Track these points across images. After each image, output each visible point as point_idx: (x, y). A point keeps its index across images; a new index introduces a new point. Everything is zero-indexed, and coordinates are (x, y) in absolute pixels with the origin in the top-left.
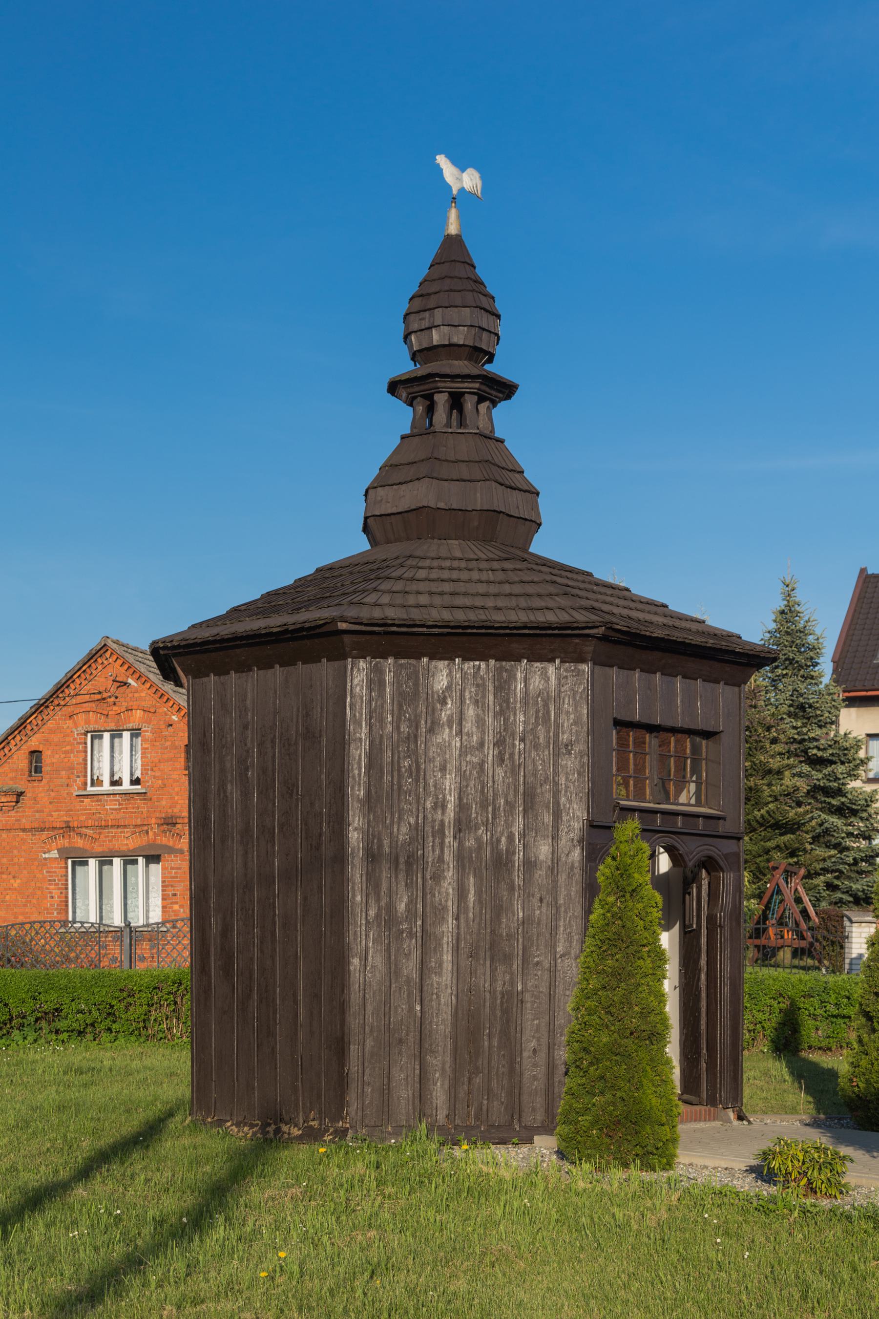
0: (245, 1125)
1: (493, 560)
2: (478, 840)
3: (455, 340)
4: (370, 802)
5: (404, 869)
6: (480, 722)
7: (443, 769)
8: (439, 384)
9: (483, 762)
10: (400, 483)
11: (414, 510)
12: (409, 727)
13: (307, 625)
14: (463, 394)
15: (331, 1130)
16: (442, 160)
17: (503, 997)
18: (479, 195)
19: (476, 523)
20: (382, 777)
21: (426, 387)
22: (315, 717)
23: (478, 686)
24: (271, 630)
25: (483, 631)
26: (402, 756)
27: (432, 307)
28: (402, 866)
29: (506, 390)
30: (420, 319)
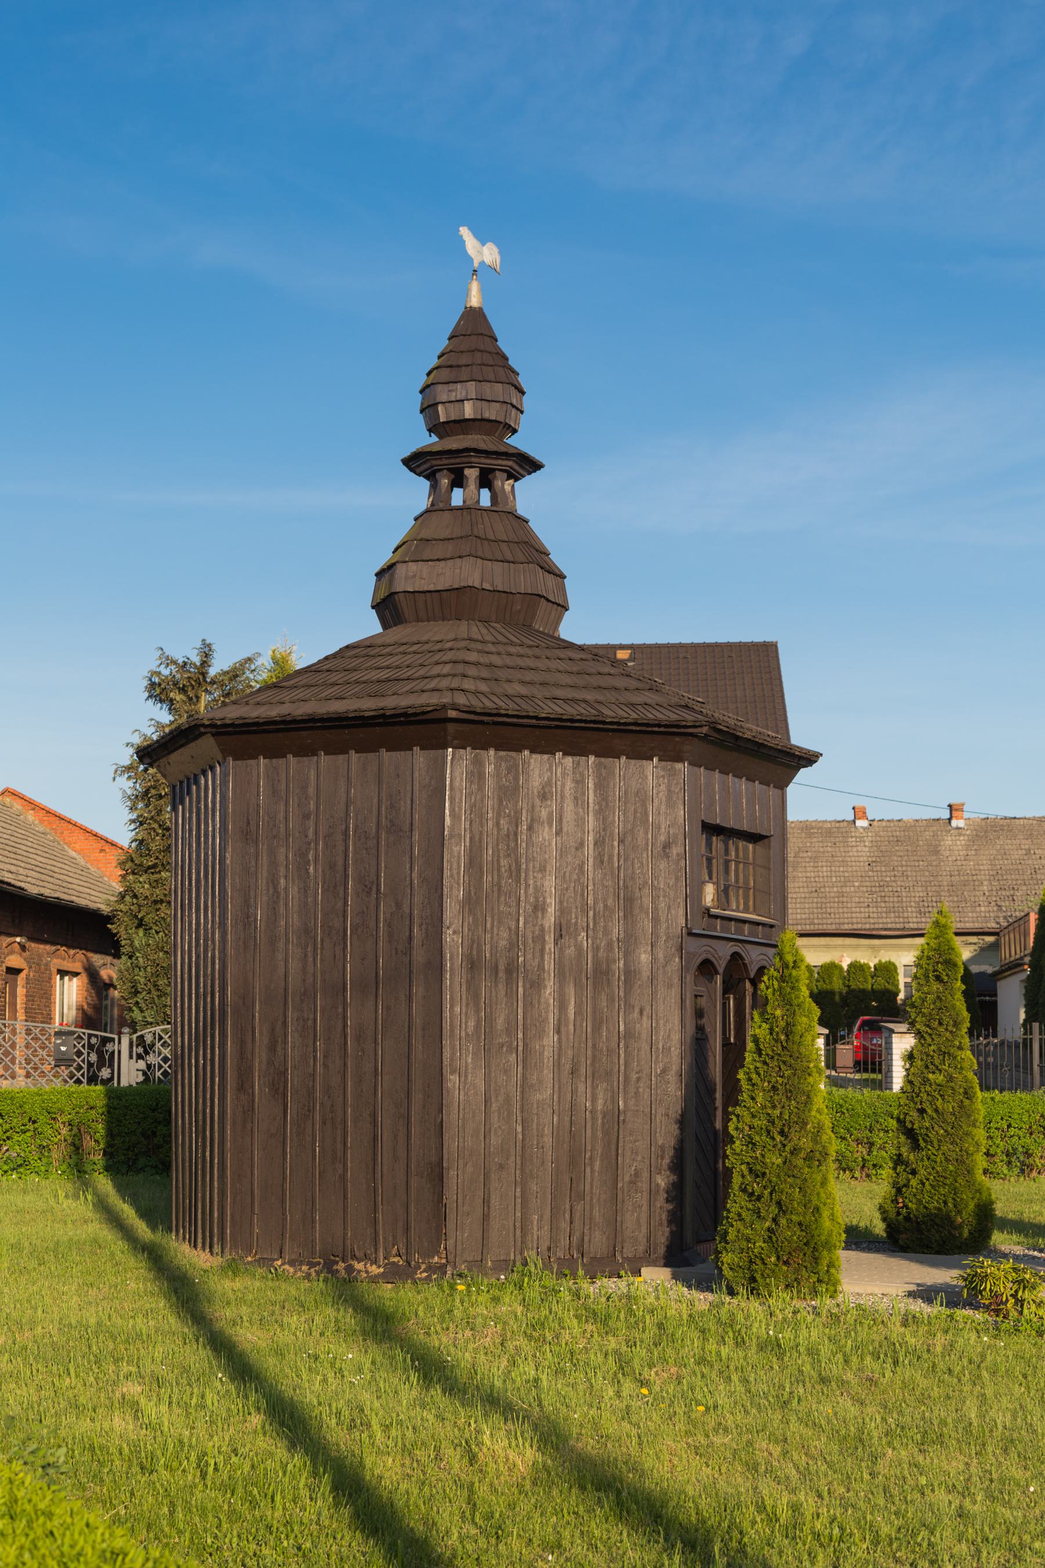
0: (301, 1263)
2: (579, 948)
3: (486, 415)
4: (470, 903)
5: (504, 977)
6: (580, 822)
7: (543, 869)
8: (473, 459)
9: (583, 863)
10: (438, 560)
11: (457, 589)
12: (510, 823)
13: (410, 711)
14: (495, 470)
15: (423, 1267)
16: (464, 232)
17: (604, 1117)
18: (498, 269)
19: (519, 607)
20: (481, 877)
21: (458, 460)
22: (403, 809)
23: (577, 782)
24: (362, 714)
25: (592, 725)
26: (501, 855)
27: (465, 379)
28: (502, 975)
29: (532, 465)
30: (450, 391)
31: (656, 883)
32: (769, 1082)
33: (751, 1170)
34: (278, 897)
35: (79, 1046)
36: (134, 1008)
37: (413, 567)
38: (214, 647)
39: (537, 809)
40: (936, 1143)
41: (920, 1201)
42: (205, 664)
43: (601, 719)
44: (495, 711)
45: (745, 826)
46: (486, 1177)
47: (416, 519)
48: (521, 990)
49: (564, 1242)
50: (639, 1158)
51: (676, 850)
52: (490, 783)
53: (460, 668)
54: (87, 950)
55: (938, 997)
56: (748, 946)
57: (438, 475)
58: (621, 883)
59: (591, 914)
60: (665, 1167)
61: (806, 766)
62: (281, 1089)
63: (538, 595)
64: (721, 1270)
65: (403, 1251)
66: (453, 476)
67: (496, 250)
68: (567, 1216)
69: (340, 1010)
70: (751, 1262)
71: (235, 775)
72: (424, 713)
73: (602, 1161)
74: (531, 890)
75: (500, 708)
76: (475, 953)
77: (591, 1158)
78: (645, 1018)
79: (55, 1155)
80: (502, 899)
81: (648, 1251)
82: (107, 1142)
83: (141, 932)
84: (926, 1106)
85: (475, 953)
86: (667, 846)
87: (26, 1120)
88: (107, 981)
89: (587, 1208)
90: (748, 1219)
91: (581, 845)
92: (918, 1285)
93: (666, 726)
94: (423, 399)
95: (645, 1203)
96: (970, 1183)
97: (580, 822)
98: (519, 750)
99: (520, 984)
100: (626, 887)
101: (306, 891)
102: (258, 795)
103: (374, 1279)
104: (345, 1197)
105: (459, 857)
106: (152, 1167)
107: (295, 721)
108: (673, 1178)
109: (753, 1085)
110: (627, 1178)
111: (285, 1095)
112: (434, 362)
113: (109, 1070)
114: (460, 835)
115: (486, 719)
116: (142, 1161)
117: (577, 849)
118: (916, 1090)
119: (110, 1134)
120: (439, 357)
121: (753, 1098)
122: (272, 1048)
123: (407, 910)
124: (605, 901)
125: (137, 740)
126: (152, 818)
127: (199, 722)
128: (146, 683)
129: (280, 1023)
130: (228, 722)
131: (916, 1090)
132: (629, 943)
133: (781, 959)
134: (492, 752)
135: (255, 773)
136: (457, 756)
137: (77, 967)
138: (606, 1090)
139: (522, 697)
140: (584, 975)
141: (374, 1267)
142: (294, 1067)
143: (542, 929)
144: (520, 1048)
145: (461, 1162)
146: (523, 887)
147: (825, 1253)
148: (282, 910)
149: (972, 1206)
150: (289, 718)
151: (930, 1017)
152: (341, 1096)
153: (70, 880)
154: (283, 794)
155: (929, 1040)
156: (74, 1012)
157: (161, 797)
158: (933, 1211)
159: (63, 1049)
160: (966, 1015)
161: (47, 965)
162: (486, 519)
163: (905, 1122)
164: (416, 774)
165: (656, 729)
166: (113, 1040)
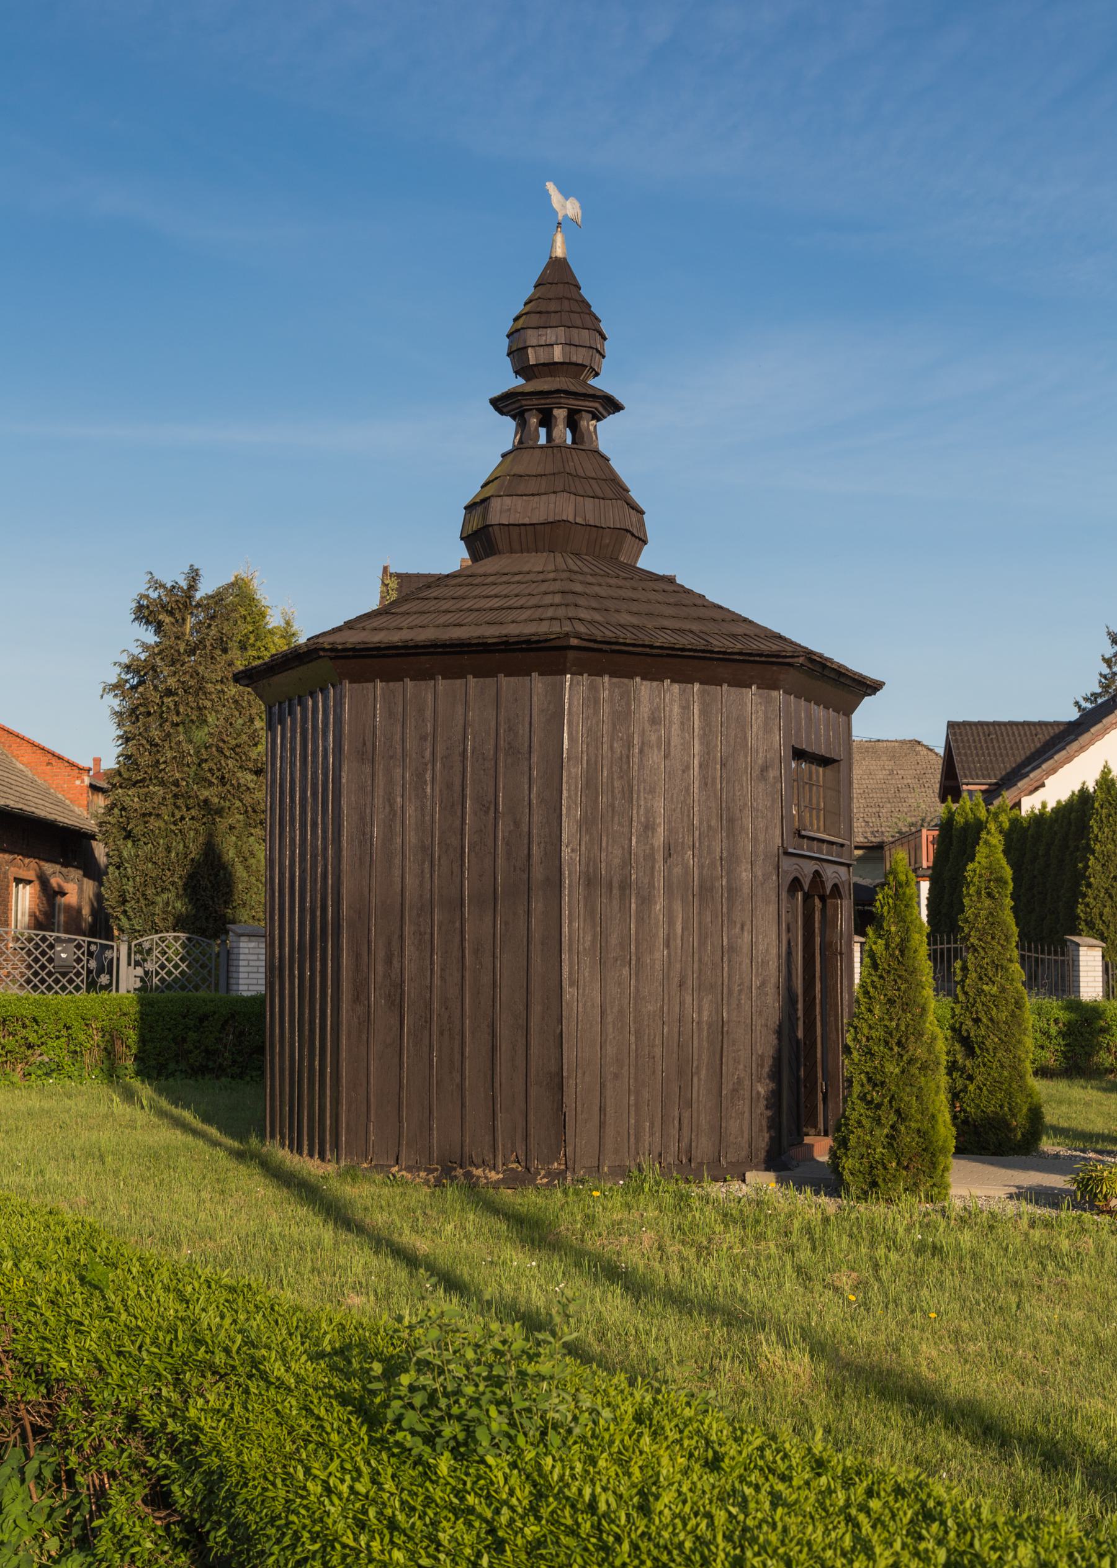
0: (419, 1169)
1: (575, 572)
2: (686, 867)
3: (574, 359)
4: (587, 823)
7: (652, 791)
9: (689, 785)
10: (533, 495)
13: (534, 638)
14: (581, 411)
15: (543, 1173)
16: (550, 187)
17: (709, 1028)
20: (597, 798)
21: (548, 401)
22: (521, 732)
28: (615, 891)
29: (612, 406)
31: (755, 805)
32: (885, 995)
33: (869, 1079)
34: (395, 815)
35: (79, 953)
36: (122, 917)
37: (508, 501)
38: (201, 572)
39: (647, 733)
40: (991, 1051)
41: (978, 1106)
42: (192, 587)
43: (709, 648)
44: (614, 640)
45: (823, 751)
46: (602, 1085)
47: (504, 456)
48: (633, 906)
49: (673, 1148)
50: (741, 1067)
51: (772, 774)
52: (605, 710)
53: (571, 598)
54: (40, 859)
55: (991, 913)
56: (825, 865)
57: (527, 415)
58: (724, 805)
59: (697, 833)
60: (765, 1075)
61: (870, 695)
62: (398, 1001)
63: (627, 531)
64: (840, 1175)
65: (522, 1158)
66: (541, 416)
67: (577, 205)
68: (676, 1123)
69: (458, 924)
70: (871, 1167)
71: (351, 698)
72: (546, 641)
73: (707, 1070)
74: (642, 811)
75: (618, 637)
76: (591, 870)
77: (697, 1067)
78: (746, 934)
79: (87, 1059)
80: (616, 818)
81: (750, 1156)
82: (139, 1048)
83: (130, 844)
84: (982, 1015)
85: (591, 870)
86: (764, 769)
87: (61, 1027)
88: (57, 889)
89: (695, 1115)
90: (868, 1126)
91: (687, 768)
92: (1018, 1187)
93: (767, 656)
94: (511, 342)
95: (747, 1109)
96: (1023, 1088)
97: (686, 746)
98: (631, 677)
99: (633, 901)
100: (728, 808)
101: (422, 810)
102: (375, 716)
103: (496, 1185)
104: (463, 1105)
105: (576, 779)
106: (181, 1071)
107: (417, 647)
108: (772, 1086)
109: (870, 998)
110: (730, 1086)
111: (401, 1007)
112: (519, 308)
113: (108, 977)
114: (577, 757)
115: (604, 647)
116: (172, 1066)
117: (683, 771)
118: (971, 1000)
119: (142, 1040)
120: (526, 304)
121: (870, 1011)
122: (389, 961)
123: (526, 829)
124: (708, 821)
125: (125, 659)
126: (140, 734)
127: (320, 646)
128: (134, 605)
129: (396, 936)
130: (349, 646)
131: (971, 1000)
132: (730, 861)
133: (895, 878)
134: (606, 678)
135: (371, 696)
136: (575, 682)
137: (31, 875)
138: (711, 1001)
139: (633, 626)
140: (690, 892)
141: (493, 1173)
142: (411, 979)
143: (652, 848)
144: (633, 962)
145: (580, 1071)
146: (635, 808)
147: (941, 1158)
148: (398, 828)
149: (1025, 1111)
150: (410, 643)
151: (983, 932)
152: (459, 1008)
153: (26, 792)
154: (400, 717)
155: (983, 954)
156: (27, 918)
157: (149, 714)
158: (991, 1115)
159: (64, 956)
160: (1015, 930)
161: (5, 873)
162: (575, 457)
163: (960, 1031)
164: (535, 699)
165: (758, 659)
166: (112, 947)
